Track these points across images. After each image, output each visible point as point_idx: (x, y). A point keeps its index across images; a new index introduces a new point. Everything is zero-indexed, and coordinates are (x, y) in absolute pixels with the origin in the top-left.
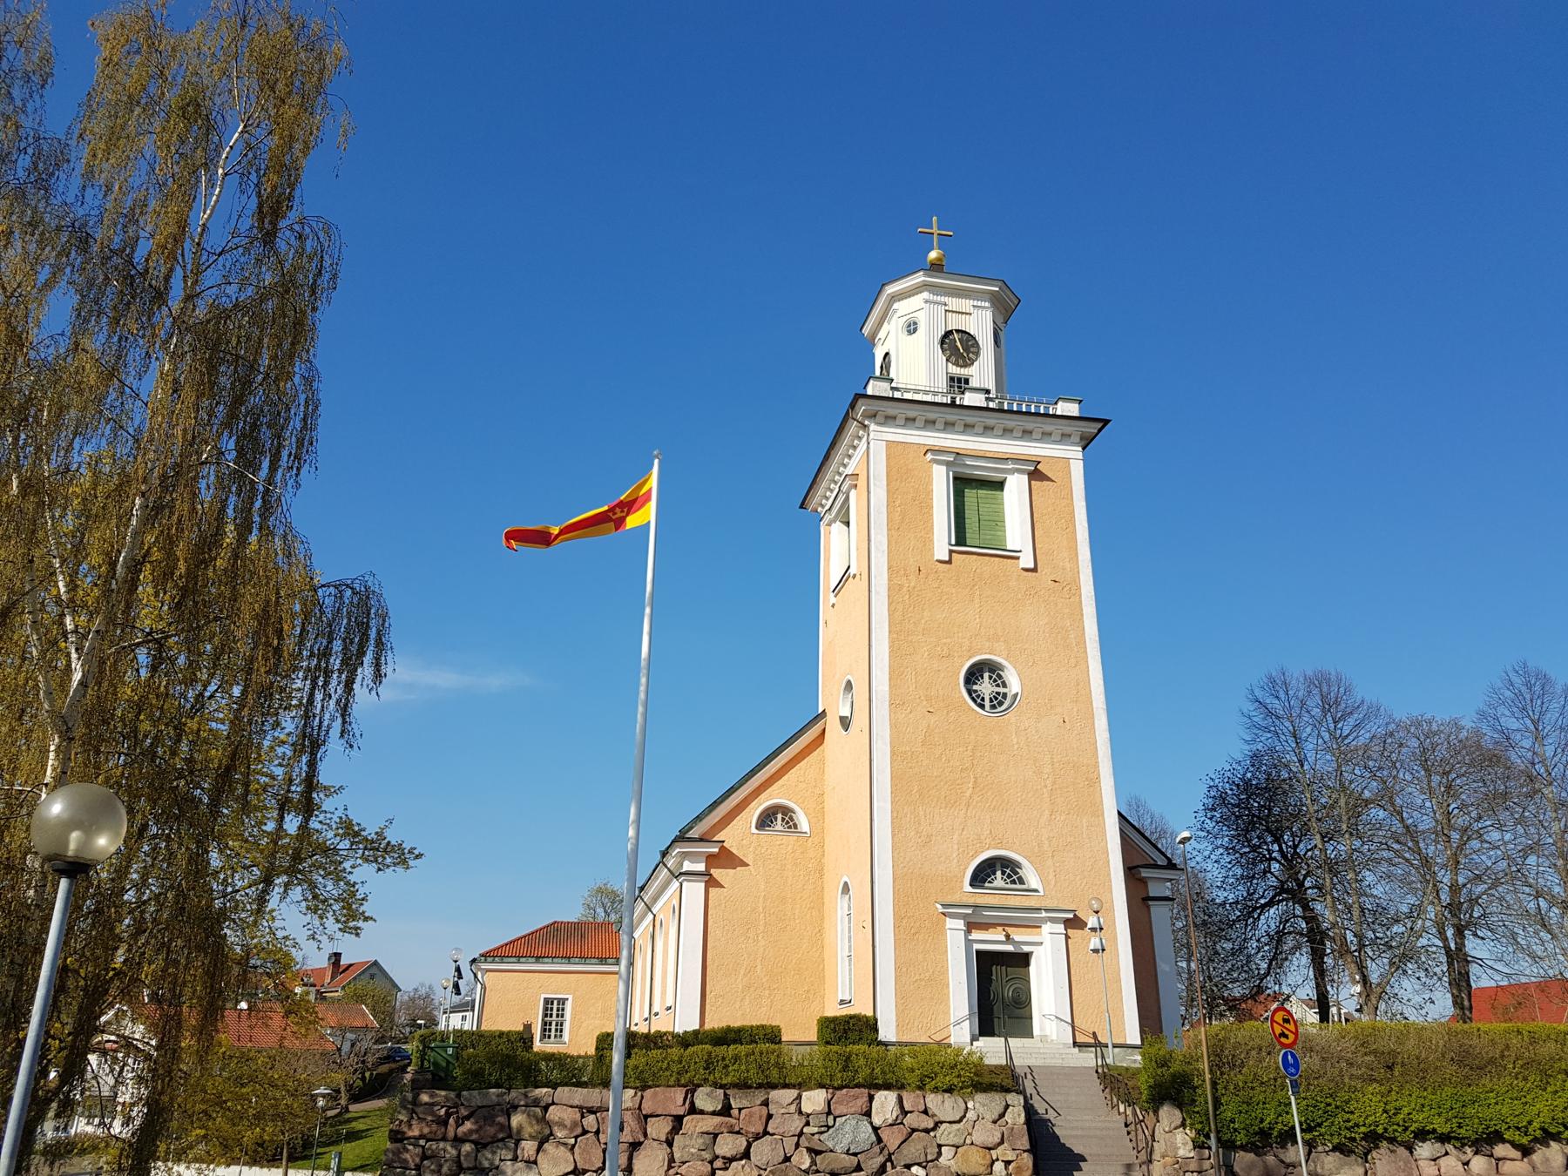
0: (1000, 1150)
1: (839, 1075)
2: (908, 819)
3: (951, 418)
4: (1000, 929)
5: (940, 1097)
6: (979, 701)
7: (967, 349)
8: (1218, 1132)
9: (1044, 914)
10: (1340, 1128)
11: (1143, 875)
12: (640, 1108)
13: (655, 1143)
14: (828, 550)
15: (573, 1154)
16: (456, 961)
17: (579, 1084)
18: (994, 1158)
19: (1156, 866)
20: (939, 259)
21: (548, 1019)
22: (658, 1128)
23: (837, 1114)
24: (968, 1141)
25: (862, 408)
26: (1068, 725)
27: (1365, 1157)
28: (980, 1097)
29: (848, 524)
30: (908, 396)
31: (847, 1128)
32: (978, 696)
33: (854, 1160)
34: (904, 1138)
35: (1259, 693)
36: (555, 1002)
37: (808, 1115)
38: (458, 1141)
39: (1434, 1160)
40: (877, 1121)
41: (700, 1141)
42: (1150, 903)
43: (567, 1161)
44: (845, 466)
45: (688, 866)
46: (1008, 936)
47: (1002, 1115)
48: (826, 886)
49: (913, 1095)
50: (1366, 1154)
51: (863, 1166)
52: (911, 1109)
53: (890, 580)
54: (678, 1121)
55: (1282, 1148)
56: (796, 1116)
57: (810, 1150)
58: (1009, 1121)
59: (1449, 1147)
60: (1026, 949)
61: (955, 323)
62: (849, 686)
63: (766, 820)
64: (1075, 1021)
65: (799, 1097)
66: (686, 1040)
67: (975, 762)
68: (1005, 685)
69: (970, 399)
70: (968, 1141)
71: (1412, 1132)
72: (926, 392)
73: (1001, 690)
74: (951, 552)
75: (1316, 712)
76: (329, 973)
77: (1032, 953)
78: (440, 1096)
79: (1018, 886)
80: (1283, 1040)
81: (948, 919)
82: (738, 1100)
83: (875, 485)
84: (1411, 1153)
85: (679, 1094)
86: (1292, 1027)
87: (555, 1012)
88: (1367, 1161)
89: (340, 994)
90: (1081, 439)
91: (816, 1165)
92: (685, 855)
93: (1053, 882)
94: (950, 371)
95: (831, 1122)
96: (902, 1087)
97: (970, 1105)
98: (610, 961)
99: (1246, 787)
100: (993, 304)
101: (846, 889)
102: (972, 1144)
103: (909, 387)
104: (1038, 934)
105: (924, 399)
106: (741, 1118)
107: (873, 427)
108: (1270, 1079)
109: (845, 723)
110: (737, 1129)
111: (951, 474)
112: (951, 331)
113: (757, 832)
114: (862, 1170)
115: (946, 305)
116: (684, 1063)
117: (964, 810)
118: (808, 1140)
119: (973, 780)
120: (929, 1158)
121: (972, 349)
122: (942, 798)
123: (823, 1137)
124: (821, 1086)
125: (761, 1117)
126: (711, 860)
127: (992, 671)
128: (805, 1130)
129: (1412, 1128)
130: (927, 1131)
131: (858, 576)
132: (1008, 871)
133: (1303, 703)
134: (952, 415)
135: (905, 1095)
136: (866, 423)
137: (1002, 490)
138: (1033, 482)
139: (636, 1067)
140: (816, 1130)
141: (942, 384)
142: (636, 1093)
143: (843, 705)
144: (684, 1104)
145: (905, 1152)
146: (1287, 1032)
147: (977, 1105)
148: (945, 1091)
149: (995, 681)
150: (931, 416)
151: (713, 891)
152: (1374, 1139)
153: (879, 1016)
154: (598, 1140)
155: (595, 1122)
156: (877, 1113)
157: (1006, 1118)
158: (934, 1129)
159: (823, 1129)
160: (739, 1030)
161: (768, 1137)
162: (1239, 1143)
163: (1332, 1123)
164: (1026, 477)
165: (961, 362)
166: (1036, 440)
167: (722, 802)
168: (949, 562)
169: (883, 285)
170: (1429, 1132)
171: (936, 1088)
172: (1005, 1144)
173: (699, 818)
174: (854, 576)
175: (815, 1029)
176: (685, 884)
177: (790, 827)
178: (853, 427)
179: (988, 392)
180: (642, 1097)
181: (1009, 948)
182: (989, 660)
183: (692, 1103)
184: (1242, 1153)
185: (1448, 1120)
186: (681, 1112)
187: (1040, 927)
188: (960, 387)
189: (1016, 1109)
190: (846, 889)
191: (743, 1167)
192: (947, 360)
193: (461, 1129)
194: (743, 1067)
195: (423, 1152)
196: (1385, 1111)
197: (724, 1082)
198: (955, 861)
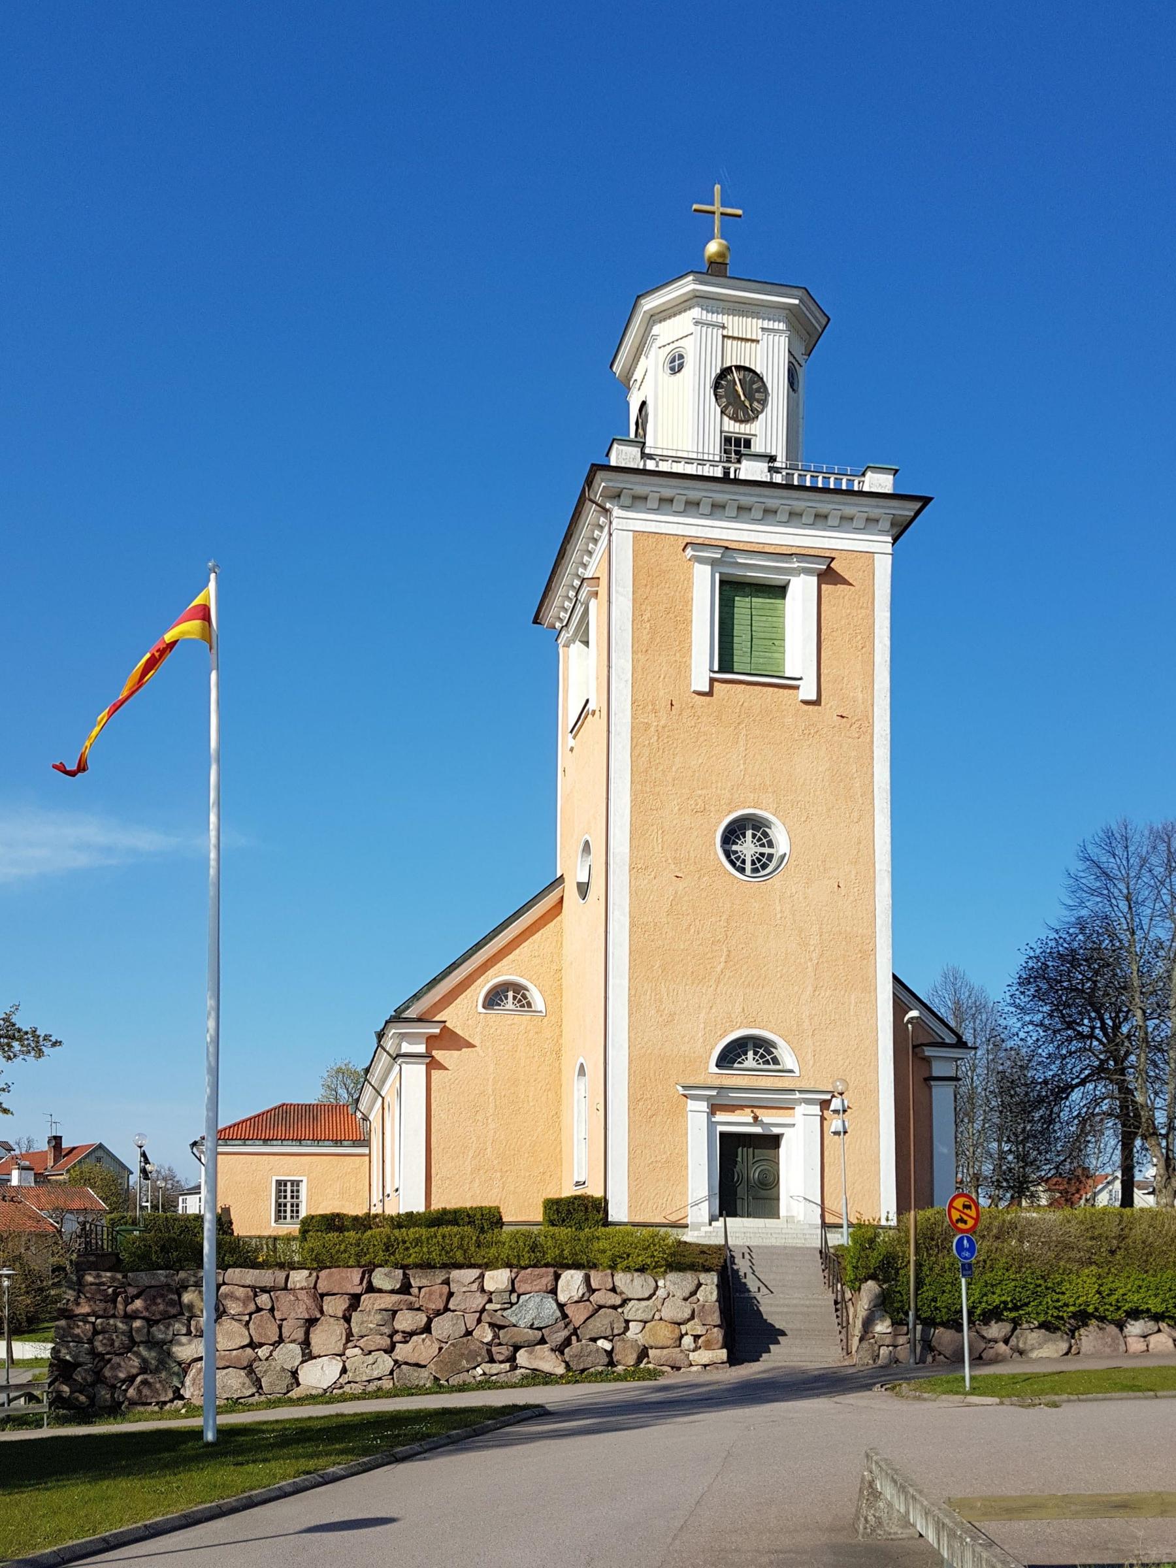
0: (689, 1326)
1: (526, 1256)
2: (648, 998)
3: (720, 498)
4: (749, 1110)
5: (629, 1276)
6: (738, 863)
7: (750, 396)
8: (917, 1310)
9: (798, 1095)
10: (1048, 1308)
11: (927, 1054)
12: (315, 1287)
13: (332, 1320)
14: (566, 679)
15: (248, 1329)
16: (141, 1147)
17: (255, 1265)
18: (683, 1332)
19: (943, 1045)
20: (721, 254)
21: (282, 1200)
22: (335, 1306)
23: (521, 1291)
24: (657, 1317)
25: (602, 483)
26: (843, 891)
27: (1072, 1333)
28: (672, 1276)
29: (586, 643)
30: (664, 467)
31: (531, 1305)
32: (738, 858)
33: (539, 1334)
34: (590, 1314)
35: (1093, 851)
36: (289, 1184)
37: (491, 1293)
38: (129, 1317)
39: (1145, 1337)
40: (562, 1298)
41: (379, 1317)
42: (932, 1083)
43: (242, 1335)
44: (585, 566)
45: (406, 1048)
46: (756, 1118)
47: (694, 1293)
48: (563, 1068)
49: (600, 1274)
50: (1073, 1332)
51: (547, 1339)
52: (597, 1287)
53: (634, 717)
54: (355, 1300)
55: (985, 1325)
56: (478, 1294)
57: (491, 1325)
58: (701, 1299)
59: (1163, 1325)
60: (776, 1131)
61: (736, 355)
62: (587, 847)
63: (494, 998)
64: (826, 1202)
65: (482, 1276)
66: (410, 1219)
67: (730, 934)
68: (771, 844)
69: (751, 470)
70: (657, 1317)
71: (1125, 1311)
72: (689, 461)
73: (766, 850)
74: (712, 680)
75: (1159, 871)
76: (51, 1157)
77: (783, 1135)
78: (106, 1277)
79: (772, 1067)
80: (960, 1225)
81: (689, 1101)
82: (417, 1280)
83: (617, 592)
84: (1121, 1330)
85: (356, 1275)
86: (973, 1213)
87: (289, 1194)
88: (1073, 1337)
89: (65, 1177)
90: (892, 525)
91: (499, 1338)
92: (403, 1037)
93: (811, 1062)
94: (726, 428)
95: (514, 1299)
96: (594, 1266)
97: (661, 1283)
98: (346, 1143)
99: (1071, 959)
100: (791, 327)
101: (582, 1071)
102: (661, 1319)
103: (680, 454)
104: (790, 1116)
105: (674, 470)
106: (421, 1296)
107: (616, 512)
108: (978, 1262)
109: (583, 889)
110: (417, 1306)
111: (717, 576)
112: (730, 368)
113: (484, 1011)
114: (546, 1343)
115: (724, 327)
116: (362, 1246)
117: (714, 986)
118: (491, 1317)
119: (725, 954)
120: (616, 1332)
121: (757, 395)
122: (689, 973)
123: (505, 1313)
124: (509, 1265)
125: (441, 1295)
126: (431, 1040)
127: (756, 828)
128: (487, 1307)
129: (1125, 1308)
130: (615, 1307)
131: (597, 713)
132: (761, 1051)
133: (1144, 861)
134: (722, 494)
135: (593, 1273)
136: (608, 506)
137: (784, 597)
138: (824, 586)
139: (312, 1250)
140: (499, 1306)
141: (714, 449)
142: (310, 1273)
143: (581, 870)
144: (361, 1283)
145: (590, 1327)
146: (965, 1218)
147: (668, 1283)
148: (637, 1270)
149: (760, 839)
150: (694, 495)
151: (435, 1074)
152: (1083, 1317)
153: (609, 1197)
154: (274, 1316)
155: (269, 1300)
156: (563, 1291)
157: (698, 1295)
158: (621, 1306)
159: (506, 1306)
160: (456, 1212)
161: (449, 1314)
162: (938, 1320)
163: (1040, 1303)
164: (815, 579)
165: (741, 414)
166: (833, 528)
167: (442, 979)
168: (710, 694)
169: (639, 297)
170: (1142, 1312)
171: (628, 1267)
172: (696, 1320)
173: (416, 997)
174: (594, 713)
175: (541, 1210)
176: (404, 1066)
177: (523, 1006)
178: (591, 513)
179: (772, 459)
180: (318, 1277)
181: (757, 1130)
182: (754, 814)
183: (370, 1282)
184: (942, 1329)
185: (1164, 1301)
186: (358, 1290)
187: (794, 1108)
188: (737, 453)
189: (708, 1288)
190: (582, 1071)
191: (424, 1340)
192: (722, 412)
193: (130, 1308)
194: (425, 1249)
195: (94, 1328)
196: (1099, 1292)
197: (405, 1262)
198: (701, 1040)
